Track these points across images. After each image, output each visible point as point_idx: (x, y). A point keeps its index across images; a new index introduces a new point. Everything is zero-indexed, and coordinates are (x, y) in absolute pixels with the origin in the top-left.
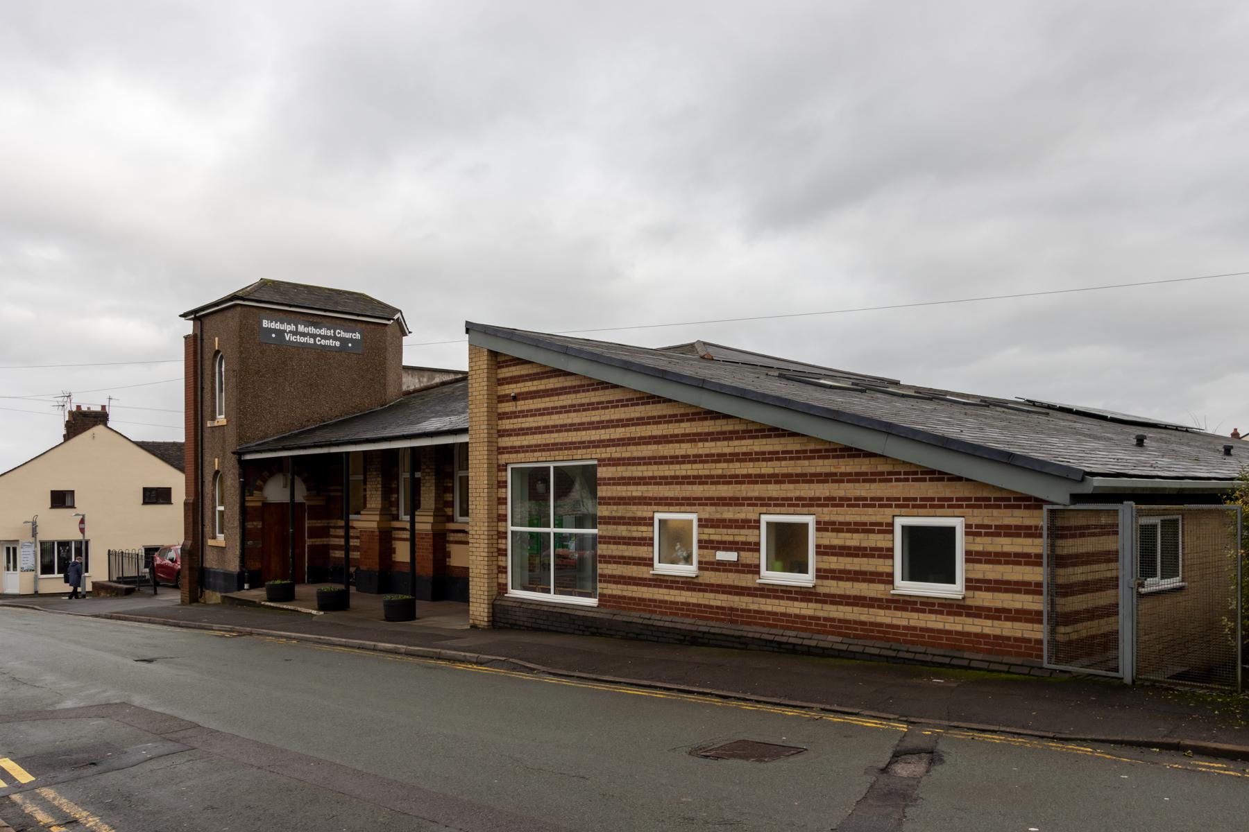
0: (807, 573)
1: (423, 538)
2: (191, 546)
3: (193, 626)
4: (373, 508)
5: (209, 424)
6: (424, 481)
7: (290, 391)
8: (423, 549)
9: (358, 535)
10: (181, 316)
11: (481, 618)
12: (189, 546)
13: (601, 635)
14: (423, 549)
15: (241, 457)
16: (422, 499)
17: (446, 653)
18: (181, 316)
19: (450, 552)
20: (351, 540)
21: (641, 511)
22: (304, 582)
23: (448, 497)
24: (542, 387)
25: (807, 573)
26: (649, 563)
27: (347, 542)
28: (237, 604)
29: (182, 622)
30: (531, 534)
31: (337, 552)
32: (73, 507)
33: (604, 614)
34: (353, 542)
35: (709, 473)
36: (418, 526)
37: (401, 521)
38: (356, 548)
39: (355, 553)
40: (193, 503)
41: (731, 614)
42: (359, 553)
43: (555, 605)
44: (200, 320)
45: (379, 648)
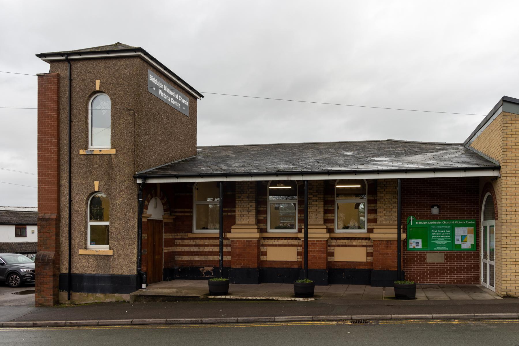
1: (316, 244)
2: (54, 256)
4: (245, 225)
5: (82, 152)
7: (160, 134)
9: (230, 244)
10: (37, 55)
12: (53, 257)
15: (145, 181)
18: (37, 55)
20: (224, 248)
22: (162, 281)
23: (262, 217)
27: (221, 249)
31: (184, 257)
32: (90, 221)
34: (225, 249)
35: (374, 209)
36: (309, 236)
37: (268, 233)
38: (229, 253)
39: (436, 261)
40: (56, 219)
42: (230, 257)
44: (69, 63)
45: (204, 322)
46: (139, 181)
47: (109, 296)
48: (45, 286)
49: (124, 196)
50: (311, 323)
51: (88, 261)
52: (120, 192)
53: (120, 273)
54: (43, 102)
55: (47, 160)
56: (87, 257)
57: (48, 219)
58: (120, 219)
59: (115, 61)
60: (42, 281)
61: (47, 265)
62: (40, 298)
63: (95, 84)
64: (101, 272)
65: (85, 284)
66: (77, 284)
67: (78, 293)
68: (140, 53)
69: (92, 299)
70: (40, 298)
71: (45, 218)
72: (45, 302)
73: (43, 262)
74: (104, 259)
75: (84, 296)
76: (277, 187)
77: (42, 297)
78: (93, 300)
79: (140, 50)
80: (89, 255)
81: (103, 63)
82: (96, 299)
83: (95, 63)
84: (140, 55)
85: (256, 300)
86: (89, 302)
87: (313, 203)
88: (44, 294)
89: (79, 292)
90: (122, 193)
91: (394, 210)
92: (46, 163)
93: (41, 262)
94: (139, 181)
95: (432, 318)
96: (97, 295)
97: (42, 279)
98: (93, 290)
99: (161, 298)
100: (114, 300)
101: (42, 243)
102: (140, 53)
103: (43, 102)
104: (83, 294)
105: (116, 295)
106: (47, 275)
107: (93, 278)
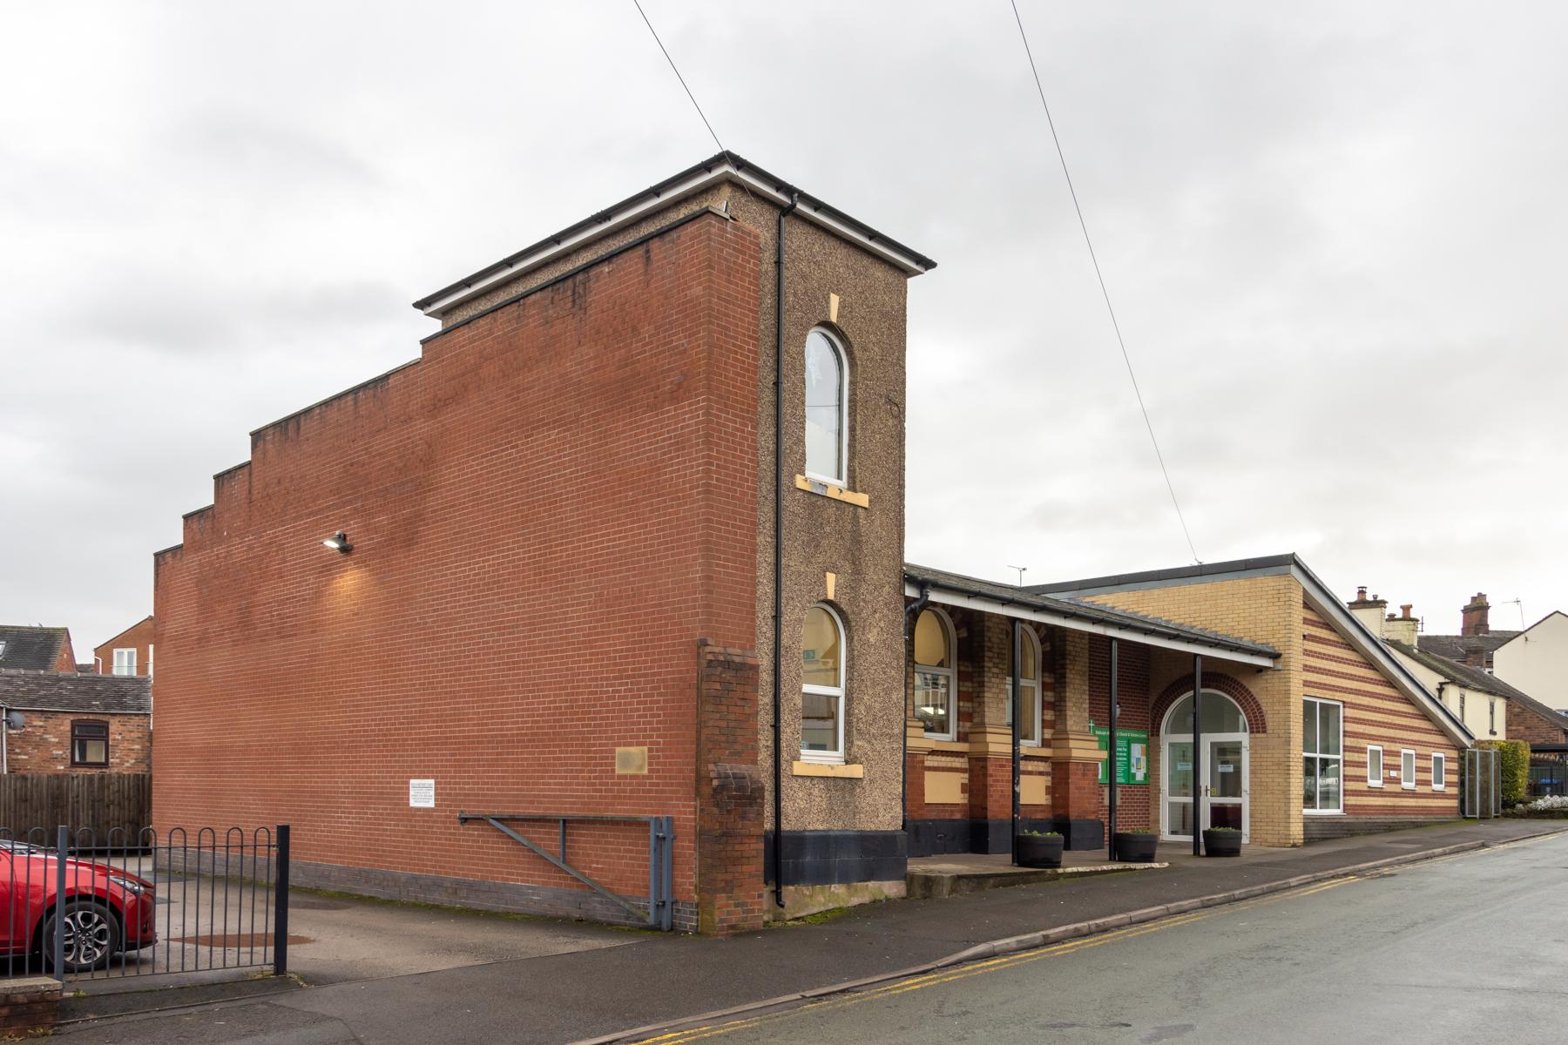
0: (1240, 805)
3: (1260, 892)
6: (990, 685)
8: (1002, 781)
11: (1298, 837)
13: (1393, 830)
14: (1002, 781)
16: (986, 709)
17: (994, 947)
19: (962, 792)
21: (1362, 743)
24: (1318, 634)
25: (1240, 805)
26: (1363, 779)
28: (996, 886)
29: (1237, 892)
30: (1328, 753)
33: (1351, 819)
41: (1394, 810)
43: (1321, 818)
46: (910, 592)
47: (856, 890)
48: (745, 868)
49: (882, 624)
50: (917, 984)
51: (810, 794)
52: (875, 612)
53: (873, 827)
54: (724, 300)
55: (733, 484)
56: (808, 783)
57: (741, 664)
58: (874, 684)
59: (866, 261)
60: (739, 853)
61: (751, 805)
62: (733, 908)
63: (828, 303)
64: (837, 826)
65: (808, 859)
66: (791, 861)
67: (791, 888)
68: (726, 168)
69: (823, 900)
70: (733, 908)
71: (733, 662)
72: (745, 920)
73: (740, 798)
74: (843, 789)
75: (804, 895)
76: (1205, 658)
77: (737, 905)
78: (824, 904)
79: (725, 157)
80: (812, 778)
81: (841, 252)
82: (829, 901)
83: (831, 244)
84: (727, 172)
85: (1096, 873)
86: (815, 910)
87: (993, 680)
88: (743, 894)
89: (793, 885)
90: (877, 615)
91: (1084, 706)
92: (729, 490)
93: (734, 797)
94: (910, 592)
95: (1128, 921)
96: (832, 889)
97: (737, 847)
98: (823, 877)
99: (992, 881)
100: (866, 899)
101: (723, 738)
102: (726, 168)
103: (724, 300)
104: (804, 888)
105: (871, 884)
106: (750, 836)
107: (826, 842)
